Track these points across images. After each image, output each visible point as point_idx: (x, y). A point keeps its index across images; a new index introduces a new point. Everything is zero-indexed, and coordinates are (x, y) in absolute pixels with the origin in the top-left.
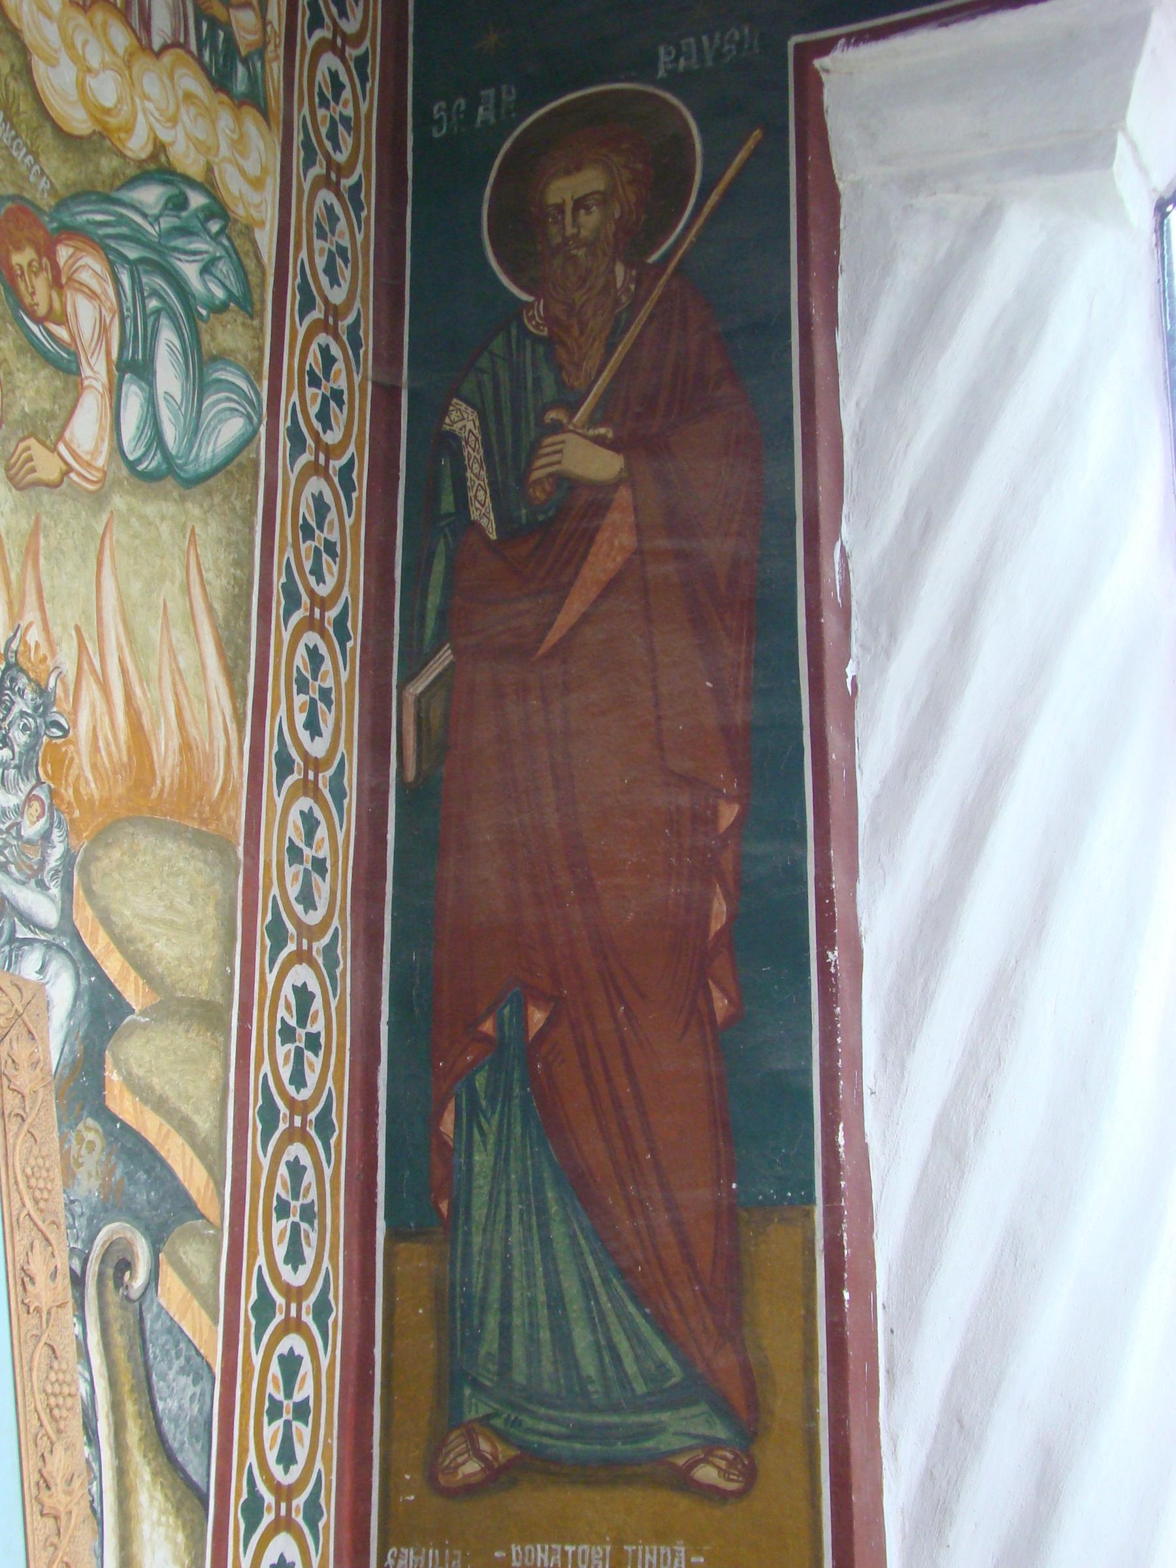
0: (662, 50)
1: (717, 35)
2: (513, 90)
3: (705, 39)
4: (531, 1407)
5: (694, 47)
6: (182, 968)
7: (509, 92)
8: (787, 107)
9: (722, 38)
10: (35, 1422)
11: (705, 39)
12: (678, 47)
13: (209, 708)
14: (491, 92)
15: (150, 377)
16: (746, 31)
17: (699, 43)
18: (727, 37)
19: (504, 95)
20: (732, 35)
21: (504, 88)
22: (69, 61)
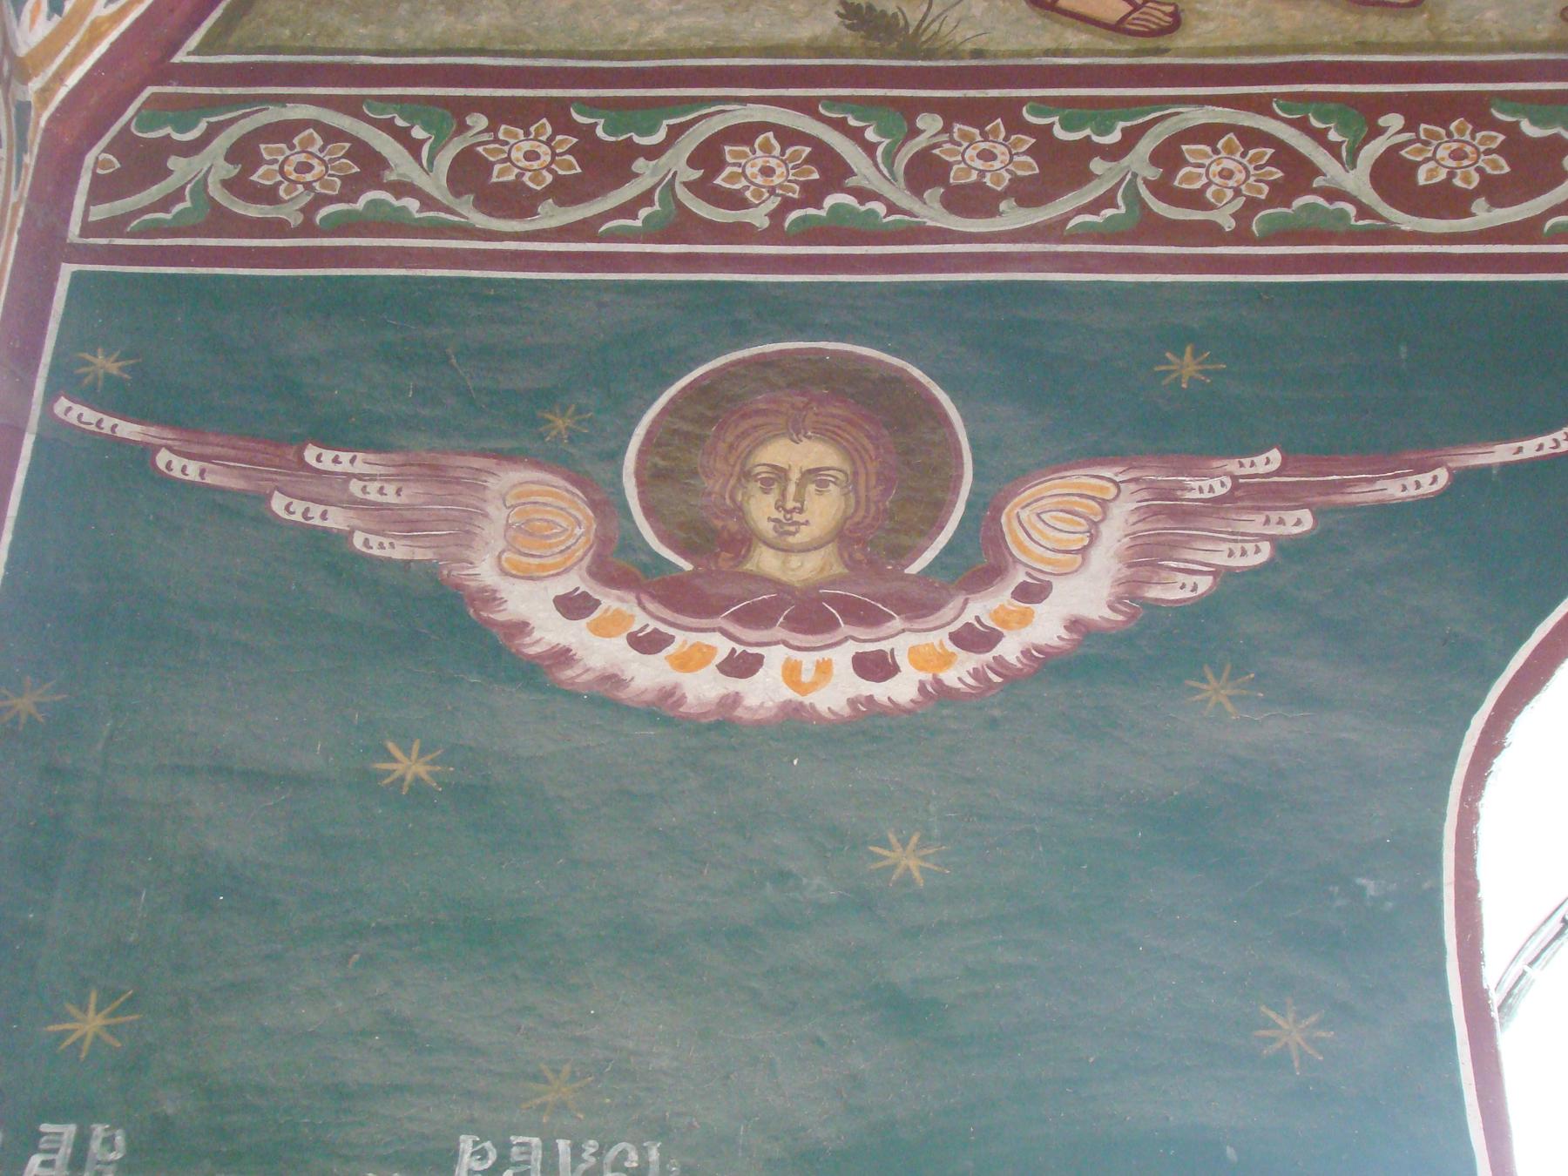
0: (466, 1143)
1: (591, 1146)
2: (120, 1139)
3: (563, 1145)
4: (969, 690)
5: (537, 1155)
6: (1030, 36)
7: (109, 1142)
8: (468, 66)
9: (599, 1154)
10: (1093, 503)
11: (563, 1145)
12: (504, 1148)
13: (1159, 544)
14: (69, 1130)
15: (729, 701)
16: (654, 1155)
17: (550, 1151)
18: (612, 1153)
19: (95, 1146)
20: (623, 1154)
21: (99, 1130)
22: (994, 650)
